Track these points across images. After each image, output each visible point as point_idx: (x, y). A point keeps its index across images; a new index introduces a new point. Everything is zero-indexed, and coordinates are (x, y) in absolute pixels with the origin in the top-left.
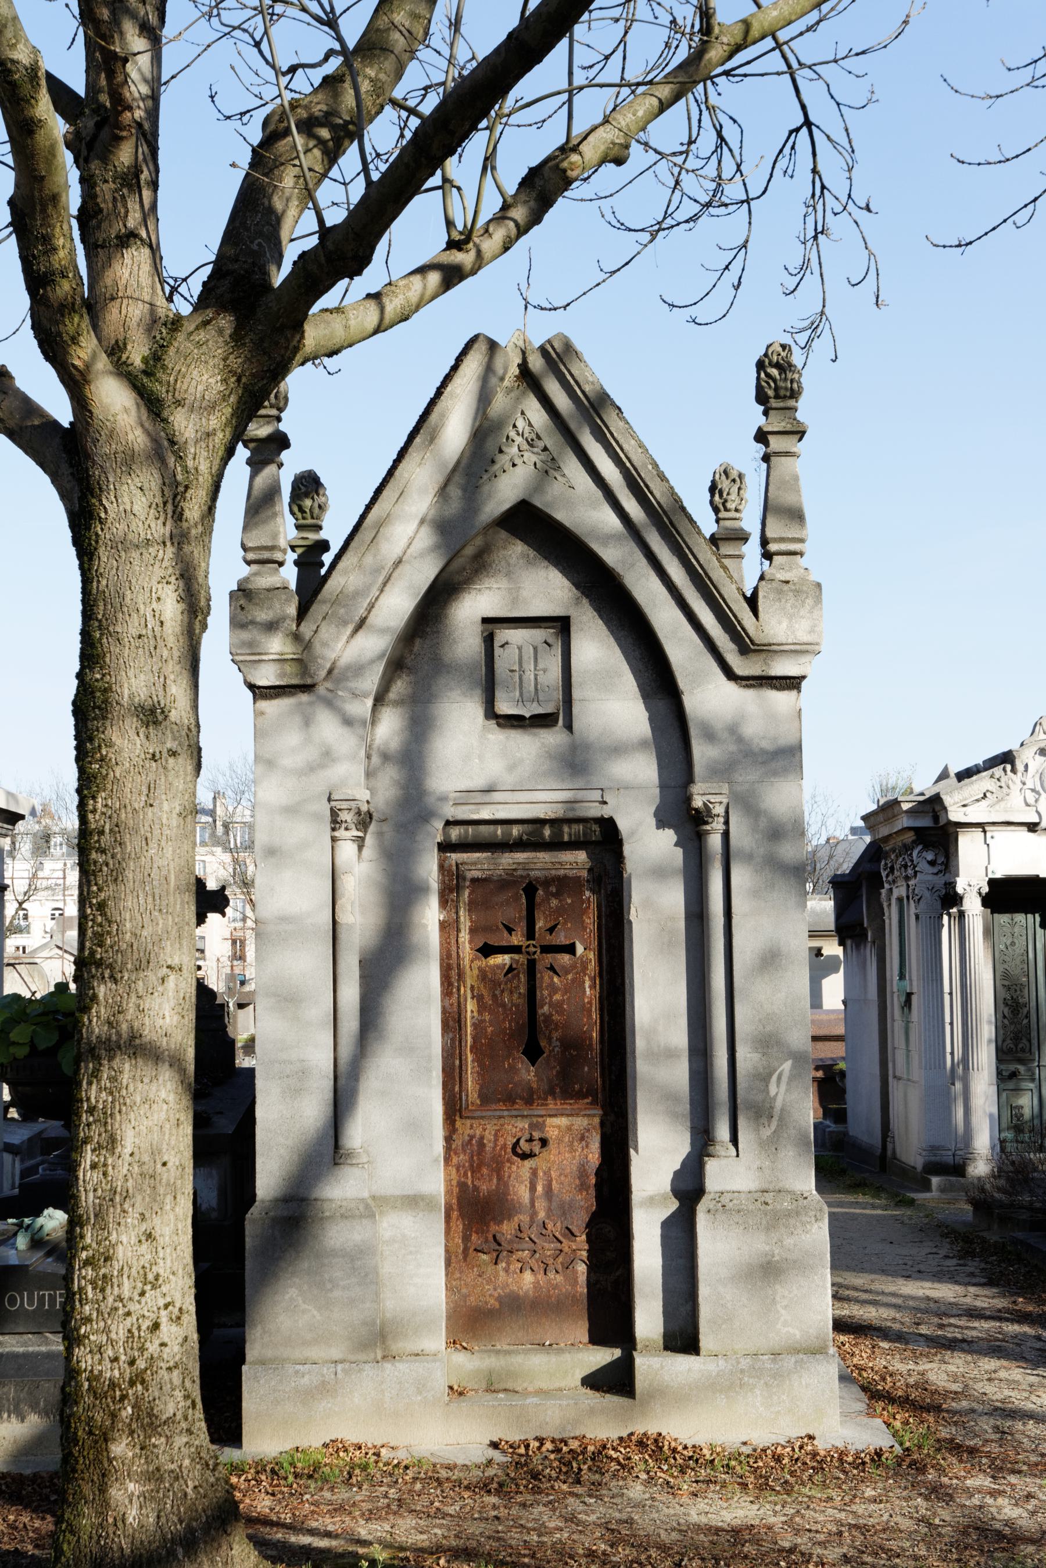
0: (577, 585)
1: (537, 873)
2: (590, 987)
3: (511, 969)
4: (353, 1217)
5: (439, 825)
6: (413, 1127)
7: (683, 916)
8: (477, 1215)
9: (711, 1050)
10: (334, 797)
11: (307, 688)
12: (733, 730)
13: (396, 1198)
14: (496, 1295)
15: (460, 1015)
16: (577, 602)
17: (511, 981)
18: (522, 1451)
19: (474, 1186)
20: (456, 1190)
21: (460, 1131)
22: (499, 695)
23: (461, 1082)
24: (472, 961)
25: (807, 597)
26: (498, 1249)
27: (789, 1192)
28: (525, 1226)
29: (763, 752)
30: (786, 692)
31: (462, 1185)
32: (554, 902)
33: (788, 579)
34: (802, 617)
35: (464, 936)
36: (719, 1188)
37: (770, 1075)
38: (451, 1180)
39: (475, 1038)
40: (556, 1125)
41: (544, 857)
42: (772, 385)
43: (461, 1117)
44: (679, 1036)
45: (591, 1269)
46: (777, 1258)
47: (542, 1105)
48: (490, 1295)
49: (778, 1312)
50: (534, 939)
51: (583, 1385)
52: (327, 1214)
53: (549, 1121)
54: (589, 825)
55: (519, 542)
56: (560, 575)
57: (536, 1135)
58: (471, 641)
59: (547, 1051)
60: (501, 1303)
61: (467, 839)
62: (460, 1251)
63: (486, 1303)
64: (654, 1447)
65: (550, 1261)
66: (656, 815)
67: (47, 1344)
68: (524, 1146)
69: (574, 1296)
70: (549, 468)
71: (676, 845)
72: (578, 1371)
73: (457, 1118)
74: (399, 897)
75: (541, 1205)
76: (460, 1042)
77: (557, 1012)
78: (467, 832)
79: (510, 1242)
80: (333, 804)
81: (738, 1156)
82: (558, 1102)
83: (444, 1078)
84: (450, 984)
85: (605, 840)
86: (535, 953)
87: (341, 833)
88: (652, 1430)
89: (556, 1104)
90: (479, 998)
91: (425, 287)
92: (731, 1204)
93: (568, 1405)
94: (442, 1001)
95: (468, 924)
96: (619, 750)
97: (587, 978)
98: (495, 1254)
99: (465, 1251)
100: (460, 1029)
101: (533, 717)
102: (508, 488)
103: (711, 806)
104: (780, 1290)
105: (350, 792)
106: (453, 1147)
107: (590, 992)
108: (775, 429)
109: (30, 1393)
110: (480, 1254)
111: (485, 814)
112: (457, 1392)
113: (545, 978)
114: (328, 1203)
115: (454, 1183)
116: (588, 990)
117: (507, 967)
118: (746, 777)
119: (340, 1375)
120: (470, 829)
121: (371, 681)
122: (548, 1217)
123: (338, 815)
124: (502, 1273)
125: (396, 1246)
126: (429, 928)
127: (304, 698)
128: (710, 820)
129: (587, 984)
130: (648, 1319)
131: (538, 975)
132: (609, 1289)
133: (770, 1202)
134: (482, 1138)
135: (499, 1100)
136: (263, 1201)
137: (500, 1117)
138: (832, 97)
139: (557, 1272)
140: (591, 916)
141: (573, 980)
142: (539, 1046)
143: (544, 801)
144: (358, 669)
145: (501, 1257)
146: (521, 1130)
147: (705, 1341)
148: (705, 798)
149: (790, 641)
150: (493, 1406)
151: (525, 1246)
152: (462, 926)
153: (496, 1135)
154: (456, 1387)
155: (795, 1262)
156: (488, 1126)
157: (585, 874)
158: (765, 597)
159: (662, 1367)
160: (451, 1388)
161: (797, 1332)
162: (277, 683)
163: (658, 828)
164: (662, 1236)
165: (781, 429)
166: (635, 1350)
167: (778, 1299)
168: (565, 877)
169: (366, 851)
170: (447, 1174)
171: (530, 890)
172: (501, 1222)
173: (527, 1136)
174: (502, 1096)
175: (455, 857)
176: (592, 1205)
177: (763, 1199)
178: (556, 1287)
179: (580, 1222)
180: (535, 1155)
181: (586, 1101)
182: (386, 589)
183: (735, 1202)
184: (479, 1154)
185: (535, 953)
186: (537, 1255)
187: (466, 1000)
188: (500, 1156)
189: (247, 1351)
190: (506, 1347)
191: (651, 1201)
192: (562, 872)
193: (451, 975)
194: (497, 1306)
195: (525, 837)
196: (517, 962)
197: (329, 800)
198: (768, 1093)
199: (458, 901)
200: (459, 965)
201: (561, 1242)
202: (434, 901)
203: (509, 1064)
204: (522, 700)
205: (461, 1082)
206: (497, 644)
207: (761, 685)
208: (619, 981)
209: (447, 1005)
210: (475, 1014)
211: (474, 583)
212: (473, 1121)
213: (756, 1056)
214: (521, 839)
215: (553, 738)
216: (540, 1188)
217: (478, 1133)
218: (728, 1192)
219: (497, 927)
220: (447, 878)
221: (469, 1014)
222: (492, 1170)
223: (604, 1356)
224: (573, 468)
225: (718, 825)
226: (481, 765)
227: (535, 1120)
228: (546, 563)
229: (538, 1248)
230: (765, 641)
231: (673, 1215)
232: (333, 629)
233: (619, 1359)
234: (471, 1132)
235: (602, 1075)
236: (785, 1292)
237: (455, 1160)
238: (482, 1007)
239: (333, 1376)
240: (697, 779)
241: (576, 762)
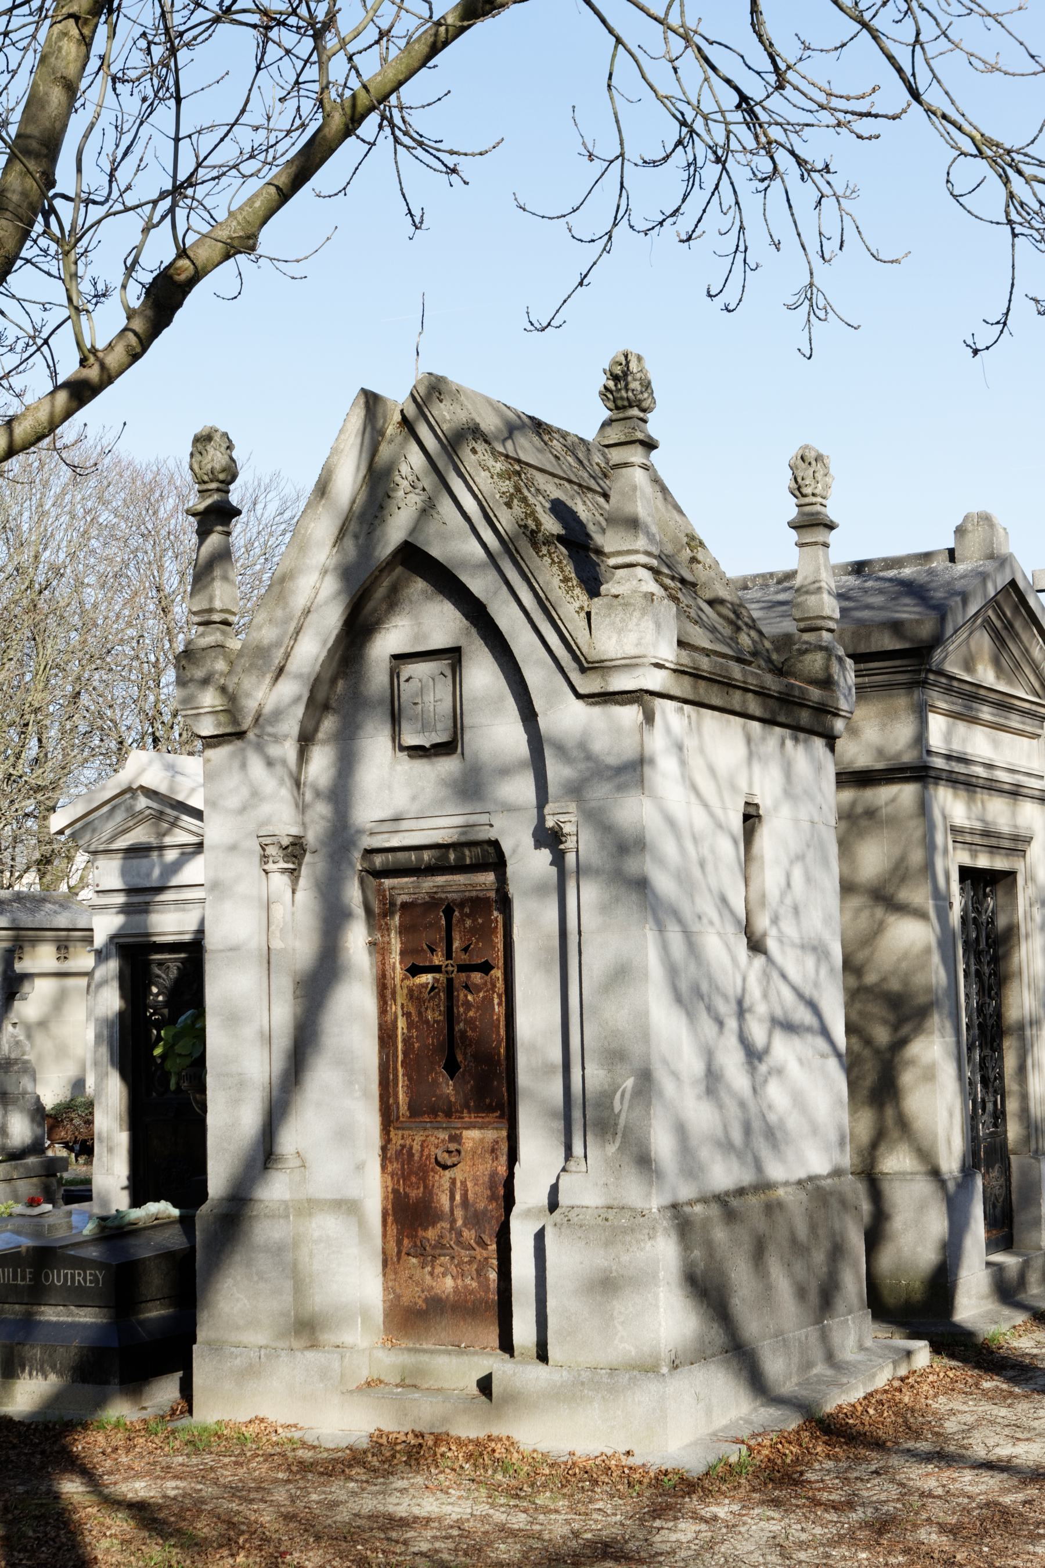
0: (467, 616)
1: (454, 896)
4: (273, 1216)
5: (357, 855)
6: (343, 1135)
11: (240, 735)
12: (583, 746)
13: (326, 1201)
16: (468, 634)
20: (391, 1196)
21: (394, 1142)
22: (405, 725)
24: (402, 981)
25: (634, 610)
26: (425, 1253)
27: (631, 1209)
29: (609, 767)
30: (628, 707)
31: (395, 1191)
32: (468, 923)
33: (617, 593)
34: (630, 631)
37: (615, 1092)
38: (387, 1187)
39: (405, 1053)
40: (472, 1137)
41: (460, 879)
42: (610, 396)
46: (614, 1274)
47: (460, 1118)
55: (419, 579)
56: (452, 607)
58: (381, 678)
59: (462, 1066)
61: (386, 867)
63: (416, 1304)
66: (534, 835)
67: (73, 1316)
70: (428, 510)
71: (551, 864)
74: (332, 921)
75: (459, 1213)
77: (471, 1029)
78: (387, 859)
79: (434, 1247)
87: (270, 866)
88: (504, 1434)
90: (407, 1015)
91: (53, 406)
95: (399, 946)
96: (505, 771)
97: (495, 996)
99: (399, 1253)
101: (435, 746)
102: (396, 530)
105: (271, 828)
108: (611, 442)
109: (50, 1356)
111: (395, 842)
115: (390, 1189)
117: (430, 986)
118: (599, 792)
119: (263, 1359)
120: (390, 856)
121: (291, 726)
125: (322, 1245)
127: (239, 744)
129: (496, 1001)
131: (456, 993)
134: (411, 1148)
135: (425, 1113)
136: (213, 1200)
138: (750, 68)
141: (484, 998)
143: (439, 827)
144: (277, 715)
149: (619, 656)
153: (422, 1146)
155: (631, 1279)
156: (416, 1138)
158: (597, 613)
159: (514, 1374)
161: (632, 1349)
162: (216, 733)
163: (536, 848)
164: (535, 1247)
165: (617, 441)
167: (615, 1314)
168: (477, 897)
170: (384, 1182)
171: (449, 912)
172: (426, 1229)
174: (427, 1109)
178: (472, 1292)
182: (299, 637)
188: (426, 1165)
189: (198, 1332)
190: (430, 1346)
191: (528, 1213)
192: (474, 894)
194: (424, 1307)
204: (423, 729)
206: (402, 679)
207: (605, 702)
210: (405, 1031)
211: (383, 623)
213: (602, 1073)
215: (448, 766)
216: (458, 1197)
217: (408, 1143)
224: (446, 506)
226: (398, 796)
228: (441, 597)
230: (597, 658)
232: (253, 679)
236: (623, 1306)
237: (390, 1169)
238: (410, 1025)
240: (550, 799)
241: (471, 787)
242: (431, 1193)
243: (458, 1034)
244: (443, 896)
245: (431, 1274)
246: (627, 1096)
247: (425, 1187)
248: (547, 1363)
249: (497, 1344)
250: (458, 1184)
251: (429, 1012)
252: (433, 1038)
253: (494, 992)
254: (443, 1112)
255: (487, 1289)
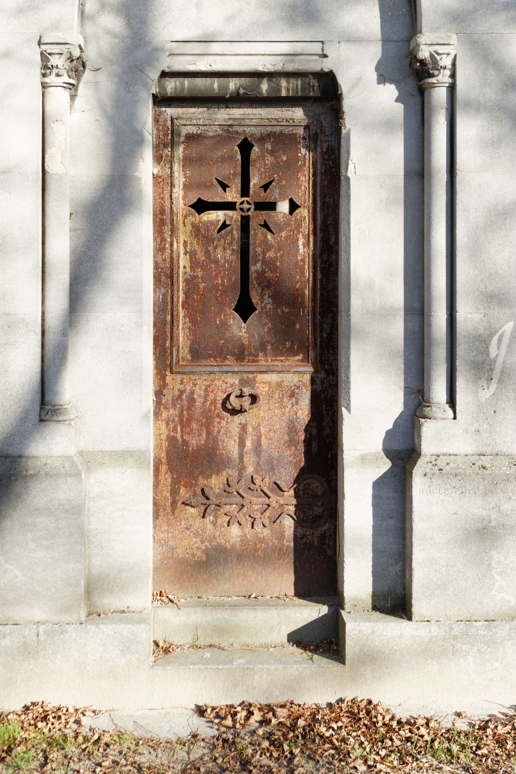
1: (254, 130)
2: (304, 244)
3: (224, 226)
4: (58, 475)
5: (155, 75)
7: (403, 173)
8: (187, 468)
9: (430, 310)
10: (45, 40)
14: (203, 548)
15: (172, 270)
17: (224, 237)
18: (229, 722)
19: (183, 440)
20: (165, 444)
23: (172, 337)
24: (185, 217)
28: (233, 481)
31: (172, 440)
35: (178, 192)
36: (435, 451)
37: (491, 336)
43: (171, 372)
44: (396, 295)
45: (299, 523)
48: (198, 548)
49: (493, 578)
50: (248, 196)
51: (289, 641)
52: (31, 472)
53: (260, 377)
54: (307, 80)
57: (247, 391)
59: (259, 308)
60: (207, 555)
61: (185, 93)
62: (168, 504)
63: (193, 555)
64: (362, 715)
65: (258, 515)
68: (234, 402)
69: (280, 549)
71: (397, 100)
72: (284, 627)
73: (168, 373)
74: (122, 147)
76: (172, 298)
77: (270, 269)
78: (182, 85)
79: (218, 496)
80: (43, 47)
81: (455, 418)
82: (269, 359)
83: (155, 333)
84: (163, 240)
85: (324, 94)
86: (249, 210)
87: (51, 79)
89: (267, 361)
92: (448, 468)
93: (276, 670)
94: (154, 256)
95: (182, 180)
97: (301, 236)
98: (203, 508)
99: (174, 503)
100: (172, 284)
103: (438, 57)
104: (496, 556)
106: (163, 401)
107: (304, 249)
110: (188, 507)
111: (202, 65)
112: (163, 650)
113: (257, 233)
114: (33, 460)
115: (164, 437)
116: (301, 247)
117: (221, 223)
119: (42, 637)
120: (187, 82)
122: (257, 472)
123: (48, 60)
124: (209, 527)
126: (143, 181)
128: (436, 72)
130: (358, 577)
131: (252, 232)
132: (316, 543)
133: (488, 466)
134: (192, 393)
135: (210, 356)
137: (211, 373)
139: (264, 526)
140: (306, 173)
141: (287, 238)
142: (252, 303)
145: (208, 510)
146: (232, 386)
147: (418, 605)
148: (432, 49)
150: (199, 669)
151: (233, 500)
152: (176, 182)
153: (206, 390)
154: (161, 644)
156: (199, 382)
157: (301, 131)
160: (156, 644)
163: (379, 83)
164: (374, 496)
166: (343, 609)
167: (493, 564)
169: (78, 100)
170: (157, 428)
171: (246, 147)
172: (209, 476)
173: (238, 393)
175: (170, 111)
176: (301, 460)
177: (480, 463)
179: (288, 478)
180: (245, 411)
181: (297, 358)
183: (452, 465)
184: (189, 409)
185: (249, 210)
186: (245, 510)
187: (178, 256)
188: (210, 411)
192: (278, 129)
193: (163, 221)
194: (204, 558)
195: (242, 91)
196: (231, 218)
197: (40, 43)
198: (488, 355)
199: (172, 157)
200: (172, 220)
201: (269, 498)
202: (147, 155)
203: (221, 320)
205: (172, 337)
208: (333, 239)
209: (160, 260)
210: (188, 270)
212: (184, 376)
213: (477, 317)
214: (238, 93)
216: (249, 444)
217: (188, 388)
218: (444, 455)
219: (212, 183)
220: (161, 133)
221: (181, 269)
222: (202, 425)
223: (312, 612)
225: (444, 77)
227: (245, 376)
229: (246, 502)
231: (385, 475)
233: (325, 615)
234: (182, 387)
235: (314, 331)
237: (165, 414)
238: (194, 263)
239: (35, 638)
242: (215, 440)
243: (254, 275)
244: (240, 129)
245: (214, 524)
246: (506, 341)
247: (208, 434)
248: (410, 619)
249: (291, 591)
250: (250, 429)
251: (219, 251)
252: (222, 278)
253: (299, 232)
254: (233, 354)
255: (282, 536)
